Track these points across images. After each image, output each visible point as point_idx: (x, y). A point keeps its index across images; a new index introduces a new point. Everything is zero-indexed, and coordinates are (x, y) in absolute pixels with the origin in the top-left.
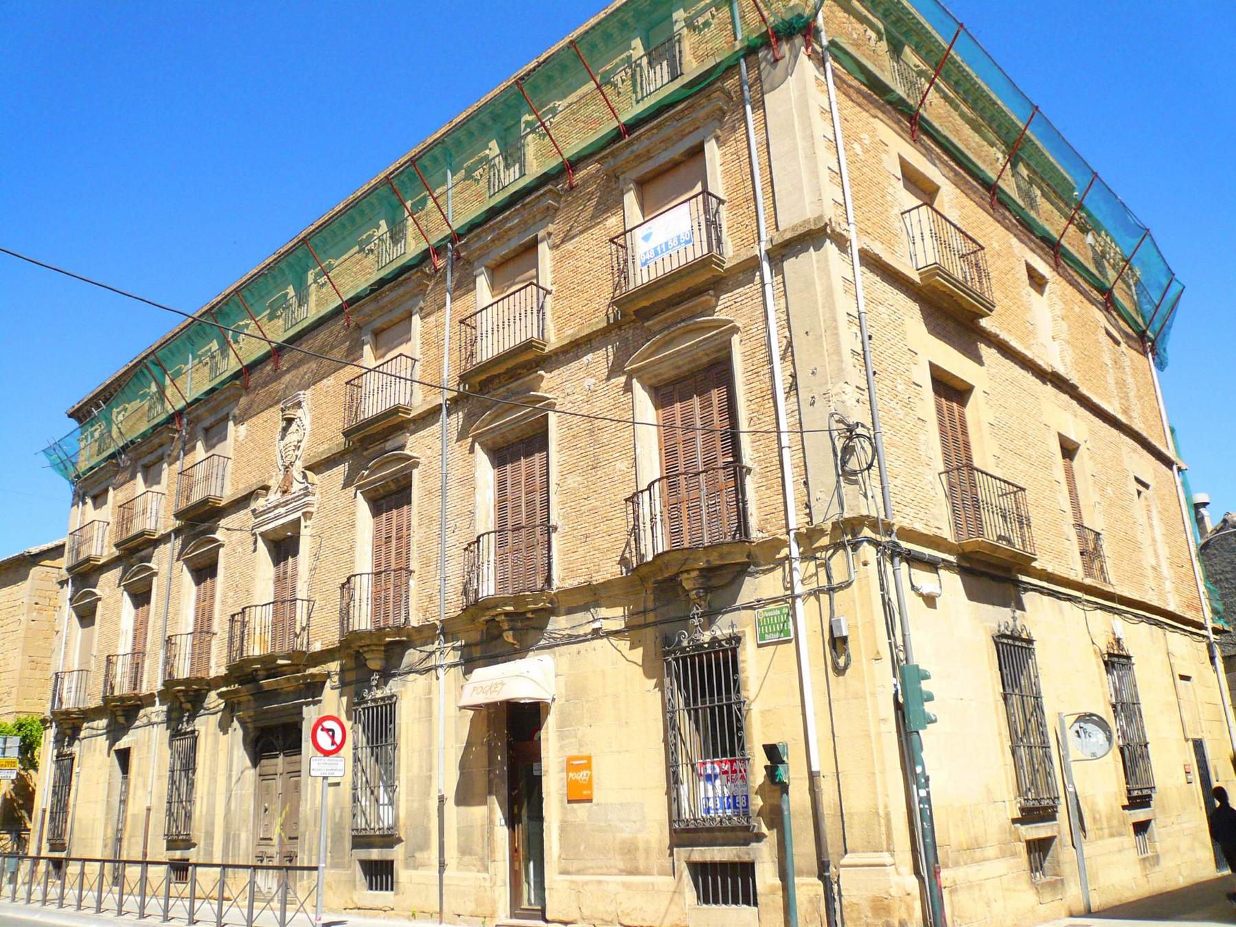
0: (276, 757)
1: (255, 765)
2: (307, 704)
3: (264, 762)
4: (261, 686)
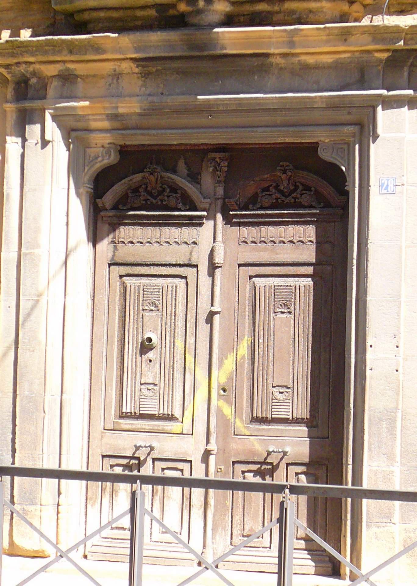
0: (196, 222)
1: (94, 238)
2: (390, 103)
3: (124, 232)
4: (212, 43)
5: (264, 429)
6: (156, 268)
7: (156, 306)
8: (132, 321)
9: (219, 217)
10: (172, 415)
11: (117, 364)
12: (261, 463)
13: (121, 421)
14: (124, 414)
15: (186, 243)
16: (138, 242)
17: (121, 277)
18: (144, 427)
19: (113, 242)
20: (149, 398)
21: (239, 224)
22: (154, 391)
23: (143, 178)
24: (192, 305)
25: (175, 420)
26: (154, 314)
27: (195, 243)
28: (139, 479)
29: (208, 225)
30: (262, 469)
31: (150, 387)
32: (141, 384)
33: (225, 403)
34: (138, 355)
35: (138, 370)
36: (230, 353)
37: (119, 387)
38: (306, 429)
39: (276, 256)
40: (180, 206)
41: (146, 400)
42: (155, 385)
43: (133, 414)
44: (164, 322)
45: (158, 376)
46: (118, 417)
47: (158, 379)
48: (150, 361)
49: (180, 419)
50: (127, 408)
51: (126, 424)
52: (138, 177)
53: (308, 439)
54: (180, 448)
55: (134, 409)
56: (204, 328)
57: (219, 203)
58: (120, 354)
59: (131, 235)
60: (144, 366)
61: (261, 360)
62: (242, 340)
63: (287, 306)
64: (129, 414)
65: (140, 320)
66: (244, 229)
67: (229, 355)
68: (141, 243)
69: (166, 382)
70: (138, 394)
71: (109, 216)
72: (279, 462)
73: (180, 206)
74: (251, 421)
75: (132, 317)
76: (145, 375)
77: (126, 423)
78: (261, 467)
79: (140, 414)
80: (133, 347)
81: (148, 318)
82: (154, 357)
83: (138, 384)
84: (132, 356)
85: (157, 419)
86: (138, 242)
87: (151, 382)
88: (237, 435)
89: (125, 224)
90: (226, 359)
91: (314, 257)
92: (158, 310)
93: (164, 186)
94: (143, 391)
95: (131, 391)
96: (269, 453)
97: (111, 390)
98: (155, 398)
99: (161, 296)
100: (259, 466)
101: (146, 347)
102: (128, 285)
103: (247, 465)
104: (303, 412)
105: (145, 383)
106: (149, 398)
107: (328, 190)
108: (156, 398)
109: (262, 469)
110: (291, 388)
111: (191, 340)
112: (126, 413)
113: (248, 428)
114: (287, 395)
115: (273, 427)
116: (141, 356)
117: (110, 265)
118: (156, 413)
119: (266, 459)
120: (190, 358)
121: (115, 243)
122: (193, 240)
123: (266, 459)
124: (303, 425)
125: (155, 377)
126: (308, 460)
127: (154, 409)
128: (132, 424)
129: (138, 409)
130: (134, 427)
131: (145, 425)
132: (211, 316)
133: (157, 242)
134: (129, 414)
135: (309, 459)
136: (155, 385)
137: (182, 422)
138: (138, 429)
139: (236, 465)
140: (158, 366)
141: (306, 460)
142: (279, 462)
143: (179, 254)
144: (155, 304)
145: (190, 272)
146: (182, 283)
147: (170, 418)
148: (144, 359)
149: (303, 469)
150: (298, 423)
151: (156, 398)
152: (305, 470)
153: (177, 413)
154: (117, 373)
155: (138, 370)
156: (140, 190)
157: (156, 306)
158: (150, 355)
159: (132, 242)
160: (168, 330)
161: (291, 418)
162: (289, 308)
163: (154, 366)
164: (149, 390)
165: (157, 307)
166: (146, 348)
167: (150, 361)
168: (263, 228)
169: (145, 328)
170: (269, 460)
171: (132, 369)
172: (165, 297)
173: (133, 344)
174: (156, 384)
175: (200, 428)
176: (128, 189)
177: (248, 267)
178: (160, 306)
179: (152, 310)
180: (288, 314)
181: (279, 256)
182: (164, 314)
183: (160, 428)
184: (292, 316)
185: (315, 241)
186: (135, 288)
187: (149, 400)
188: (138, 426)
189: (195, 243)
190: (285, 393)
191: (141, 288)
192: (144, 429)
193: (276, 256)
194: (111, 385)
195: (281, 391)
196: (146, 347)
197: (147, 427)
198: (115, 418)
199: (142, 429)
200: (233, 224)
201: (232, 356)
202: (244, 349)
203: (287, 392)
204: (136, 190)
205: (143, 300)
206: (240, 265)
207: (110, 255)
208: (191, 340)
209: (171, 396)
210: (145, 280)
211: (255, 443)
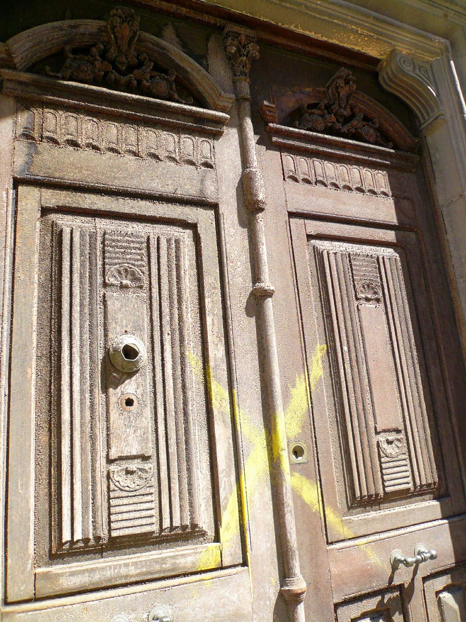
0: (209, 130)
5: (374, 519)
6: (128, 201)
7: (135, 278)
8: (77, 309)
9: (249, 124)
10: (194, 526)
11: (37, 416)
12: (381, 592)
13: (56, 569)
14: (67, 546)
15: (191, 163)
16: (88, 145)
17: (45, 211)
18: (123, 571)
19: (27, 136)
20: (133, 493)
21: (281, 148)
22: (144, 475)
23: (100, 30)
24: (211, 279)
25: (199, 537)
26: (130, 294)
27: (207, 165)
28: (401, 594)
29: (231, 135)
30: (385, 601)
31: (133, 465)
32: (110, 461)
33: (304, 479)
34: (98, 390)
35: (100, 426)
36: (299, 374)
37: (45, 476)
38: (436, 503)
39: (341, 207)
40: (176, 97)
41: (125, 501)
42: (145, 458)
43: (92, 542)
44: (156, 314)
45: (151, 437)
46: (46, 559)
47: (151, 445)
48: (129, 402)
49: (211, 533)
50: (77, 527)
51: (73, 574)
52: (90, 26)
53: (446, 521)
54: (224, 606)
55: (95, 528)
56: (244, 328)
57: (247, 106)
58: (45, 389)
59: (72, 129)
60: (114, 415)
61: (350, 385)
62: (313, 349)
63: (373, 288)
64: (81, 544)
65: (99, 309)
66: (288, 159)
67: (297, 379)
68: (96, 148)
69: (173, 449)
70: (101, 487)
71: (20, 83)
72: (413, 580)
73: (176, 97)
74: (349, 508)
75: (77, 301)
76: (119, 438)
77: (71, 573)
78: (383, 598)
79: (110, 538)
80: (82, 373)
81: (118, 304)
82: (140, 391)
83: (101, 462)
84: (82, 392)
85: (153, 544)
86: (88, 145)
87: (134, 453)
88: (332, 543)
89: (56, 106)
90: (294, 386)
91: (395, 215)
92: (141, 287)
93: (142, 57)
94: (116, 477)
95: (84, 481)
96: (395, 565)
97: (26, 486)
98: (148, 490)
99: (145, 259)
100: (379, 598)
101: (117, 366)
102: (67, 232)
103: (359, 604)
104: (428, 474)
105: (121, 458)
106: (133, 493)
107: (395, 126)
108: (152, 490)
109: (385, 601)
110: (403, 432)
111: (217, 352)
112: (184, 527)
113: (350, 522)
114: (400, 445)
115: (387, 512)
116: (105, 390)
117: (17, 183)
118: (155, 528)
119: (391, 579)
120: (219, 391)
121: (33, 139)
122: (204, 160)
123: (391, 579)
124: (427, 497)
125: (144, 440)
126: (453, 561)
127: (149, 521)
128: (93, 570)
129: (106, 527)
130: (96, 577)
131: (127, 565)
132: (257, 301)
133: (130, 151)
134: (81, 544)
135: (456, 556)
136: (145, 458)
137: (217, 539)
138: (110, 580)
139: (339, 611)
140: (148, 412)
141: (450, 561)
142: (413, 580)
143: (185, 181)
144: (133, 274)
145: (203, 218)
146: (186, 236)
147: (189, 534)
148: (113, 399)
149: (444, 581)
150: (421, 495)
151: (152, 490)
152: (450, 582)
153: (205, 521)
154: (37, 439)
155: (100, 426)
156: (94, 50)
157: (135, 278)
158: (129, 388)
159: (74, 144)
160: (167, 329)
161: (412, 489)
162: (375, 293)
163: (139, 415)
164: (132, 473)
165: (139, 280)
166: (116, 371)
167: (129, 402)
168: (317, 162)
169: (112, 326)
170: (396, 582)
171: (82, 425)
172: (154, 260)
173: (82, 364)
174: (149, 457)
175: (263, 543)
176: (66, 43)
177: (302, 220)
178: (145, 279)
179: (126, 287)
180: (374, 302)
181: (348, 208)
182: (155, 294)
183: (168, 565)
184: (382, 305)
185: (390, 194)
186: (82, 236)
187: (135, 500)
188: (109, 574)
189: (207, 165)
190: (396, 443)
191: (99, 239)
192: (126, 577)
193: (341, 207)
194: (25, 473)
195: (390, 438)
196: (117, 366)
197: (133, 571)
198: (37, 563)
199: (121, 577)
200: (271, 146)
201: (302, 380)
202: (318, 369)
203: (398, 440)
204: (83, 50)
205: (104, 264)
206: (292, 215)
207: (20, 161)
208: (217, 352)
209: (185, 481)
210: (103, 224)
211: (369, 551)
